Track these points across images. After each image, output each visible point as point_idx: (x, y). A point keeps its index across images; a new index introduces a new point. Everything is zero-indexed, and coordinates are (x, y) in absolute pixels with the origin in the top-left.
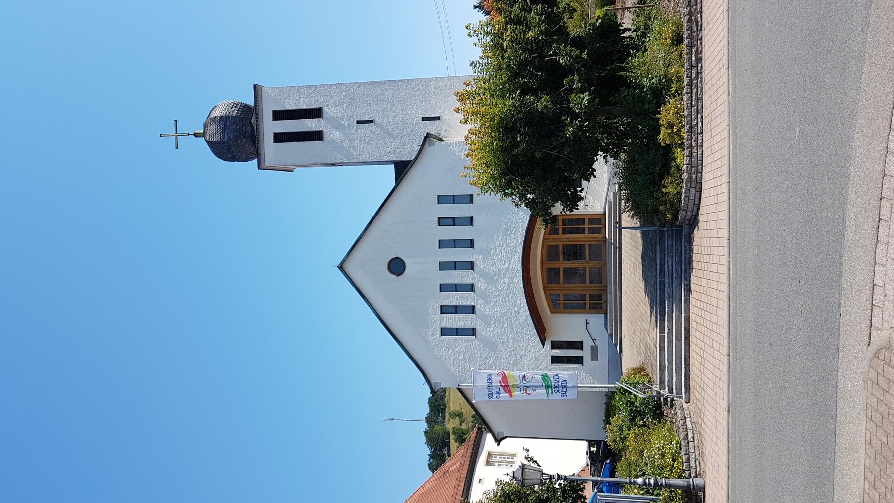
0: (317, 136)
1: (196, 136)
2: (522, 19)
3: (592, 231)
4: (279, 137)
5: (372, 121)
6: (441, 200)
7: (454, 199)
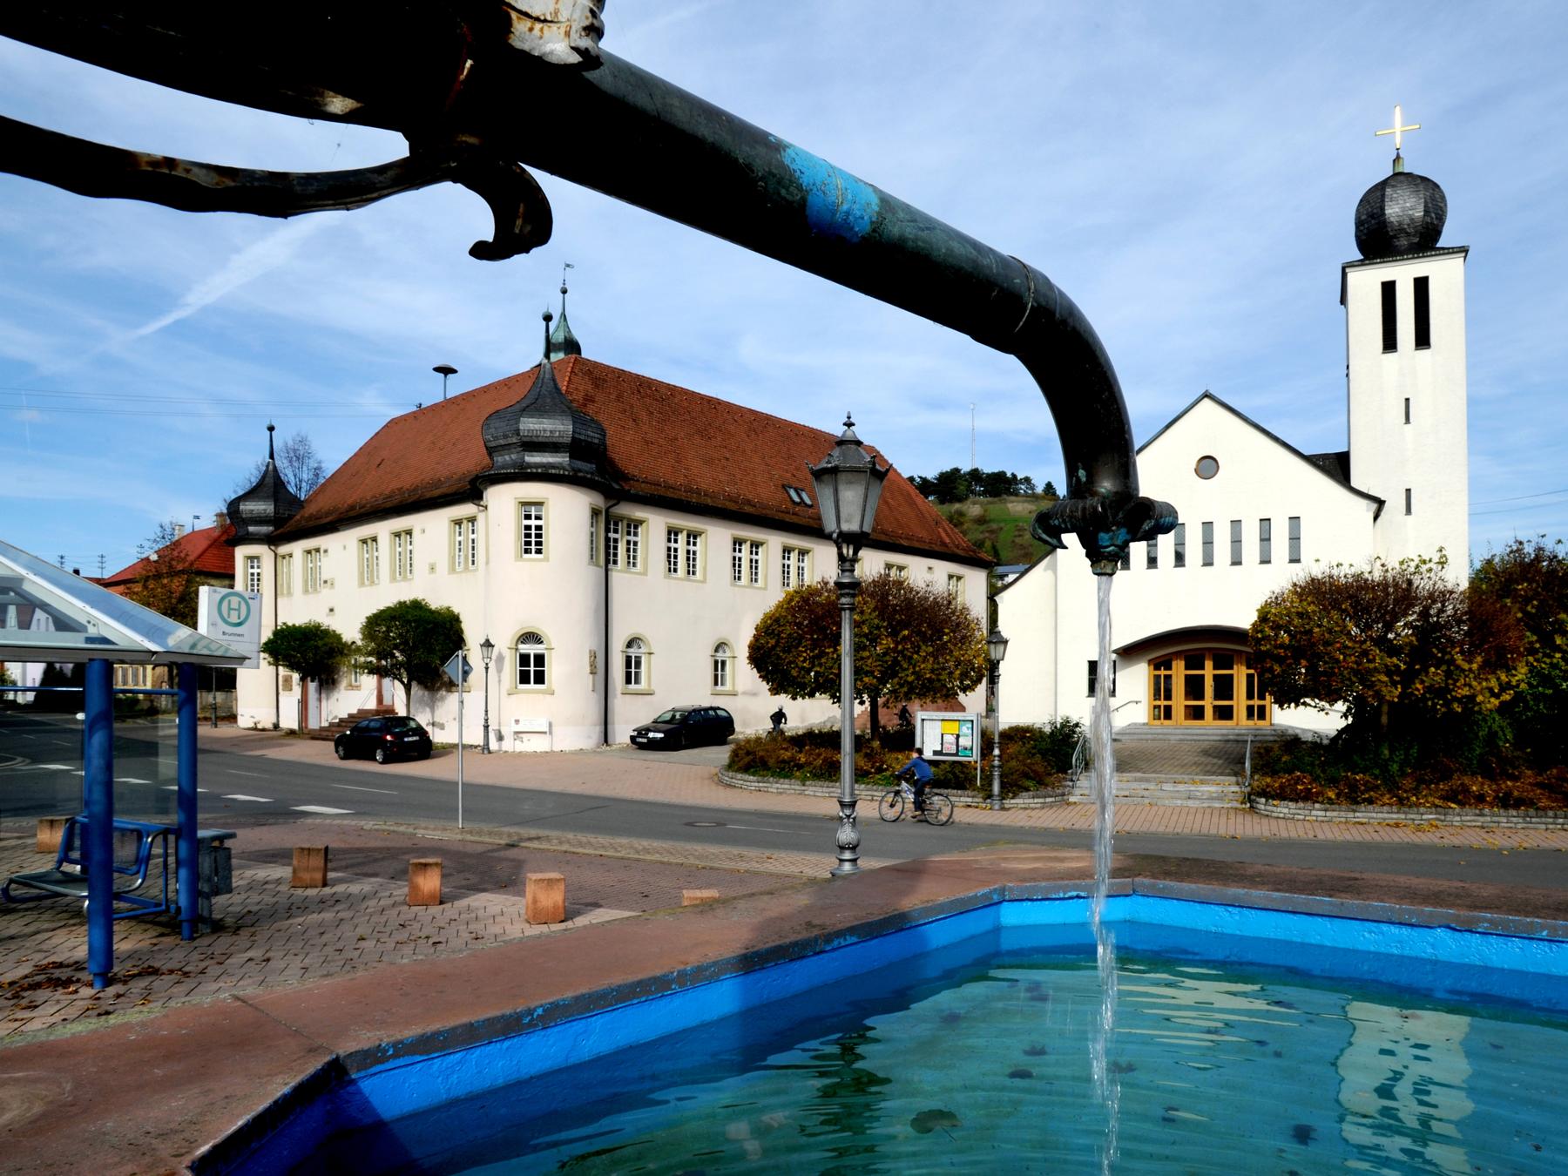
0: (1390, 343)
1: (1394, 161)
2: (1531, 623)
3: (1250, 709)
4: (1389, 289)
5: (1408, 420)
6: (1295, 520)
7: (1295, 539)
